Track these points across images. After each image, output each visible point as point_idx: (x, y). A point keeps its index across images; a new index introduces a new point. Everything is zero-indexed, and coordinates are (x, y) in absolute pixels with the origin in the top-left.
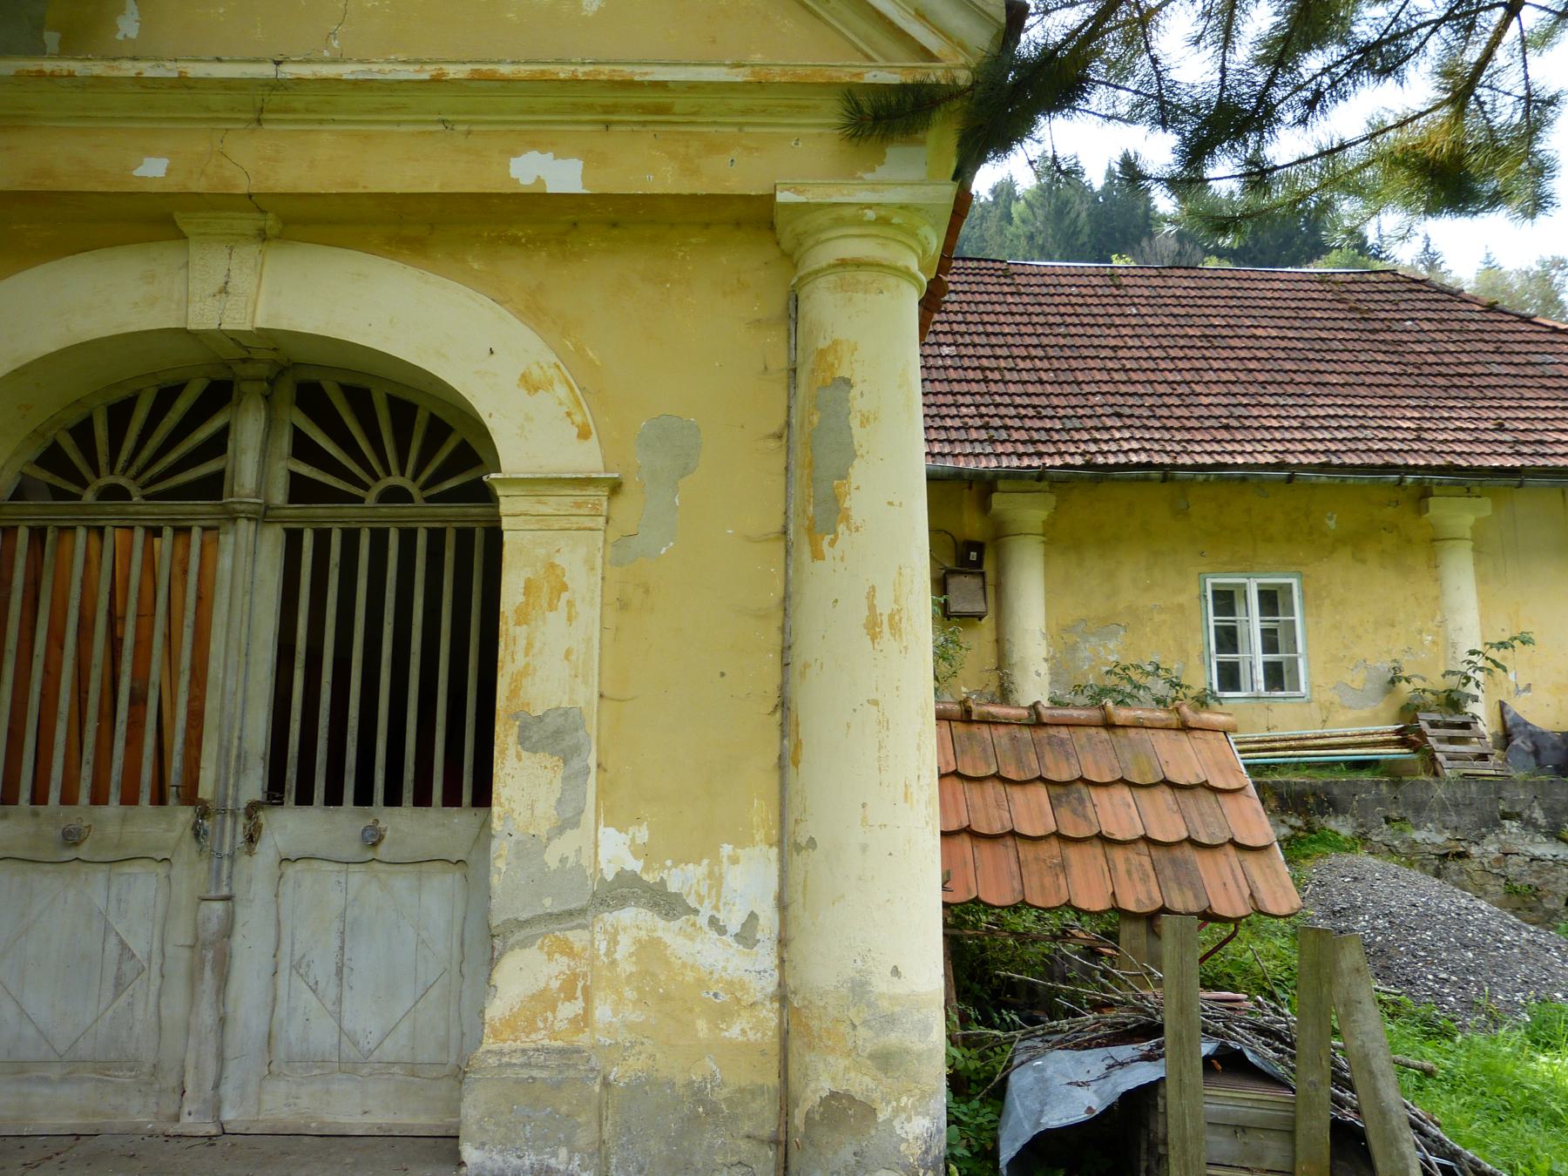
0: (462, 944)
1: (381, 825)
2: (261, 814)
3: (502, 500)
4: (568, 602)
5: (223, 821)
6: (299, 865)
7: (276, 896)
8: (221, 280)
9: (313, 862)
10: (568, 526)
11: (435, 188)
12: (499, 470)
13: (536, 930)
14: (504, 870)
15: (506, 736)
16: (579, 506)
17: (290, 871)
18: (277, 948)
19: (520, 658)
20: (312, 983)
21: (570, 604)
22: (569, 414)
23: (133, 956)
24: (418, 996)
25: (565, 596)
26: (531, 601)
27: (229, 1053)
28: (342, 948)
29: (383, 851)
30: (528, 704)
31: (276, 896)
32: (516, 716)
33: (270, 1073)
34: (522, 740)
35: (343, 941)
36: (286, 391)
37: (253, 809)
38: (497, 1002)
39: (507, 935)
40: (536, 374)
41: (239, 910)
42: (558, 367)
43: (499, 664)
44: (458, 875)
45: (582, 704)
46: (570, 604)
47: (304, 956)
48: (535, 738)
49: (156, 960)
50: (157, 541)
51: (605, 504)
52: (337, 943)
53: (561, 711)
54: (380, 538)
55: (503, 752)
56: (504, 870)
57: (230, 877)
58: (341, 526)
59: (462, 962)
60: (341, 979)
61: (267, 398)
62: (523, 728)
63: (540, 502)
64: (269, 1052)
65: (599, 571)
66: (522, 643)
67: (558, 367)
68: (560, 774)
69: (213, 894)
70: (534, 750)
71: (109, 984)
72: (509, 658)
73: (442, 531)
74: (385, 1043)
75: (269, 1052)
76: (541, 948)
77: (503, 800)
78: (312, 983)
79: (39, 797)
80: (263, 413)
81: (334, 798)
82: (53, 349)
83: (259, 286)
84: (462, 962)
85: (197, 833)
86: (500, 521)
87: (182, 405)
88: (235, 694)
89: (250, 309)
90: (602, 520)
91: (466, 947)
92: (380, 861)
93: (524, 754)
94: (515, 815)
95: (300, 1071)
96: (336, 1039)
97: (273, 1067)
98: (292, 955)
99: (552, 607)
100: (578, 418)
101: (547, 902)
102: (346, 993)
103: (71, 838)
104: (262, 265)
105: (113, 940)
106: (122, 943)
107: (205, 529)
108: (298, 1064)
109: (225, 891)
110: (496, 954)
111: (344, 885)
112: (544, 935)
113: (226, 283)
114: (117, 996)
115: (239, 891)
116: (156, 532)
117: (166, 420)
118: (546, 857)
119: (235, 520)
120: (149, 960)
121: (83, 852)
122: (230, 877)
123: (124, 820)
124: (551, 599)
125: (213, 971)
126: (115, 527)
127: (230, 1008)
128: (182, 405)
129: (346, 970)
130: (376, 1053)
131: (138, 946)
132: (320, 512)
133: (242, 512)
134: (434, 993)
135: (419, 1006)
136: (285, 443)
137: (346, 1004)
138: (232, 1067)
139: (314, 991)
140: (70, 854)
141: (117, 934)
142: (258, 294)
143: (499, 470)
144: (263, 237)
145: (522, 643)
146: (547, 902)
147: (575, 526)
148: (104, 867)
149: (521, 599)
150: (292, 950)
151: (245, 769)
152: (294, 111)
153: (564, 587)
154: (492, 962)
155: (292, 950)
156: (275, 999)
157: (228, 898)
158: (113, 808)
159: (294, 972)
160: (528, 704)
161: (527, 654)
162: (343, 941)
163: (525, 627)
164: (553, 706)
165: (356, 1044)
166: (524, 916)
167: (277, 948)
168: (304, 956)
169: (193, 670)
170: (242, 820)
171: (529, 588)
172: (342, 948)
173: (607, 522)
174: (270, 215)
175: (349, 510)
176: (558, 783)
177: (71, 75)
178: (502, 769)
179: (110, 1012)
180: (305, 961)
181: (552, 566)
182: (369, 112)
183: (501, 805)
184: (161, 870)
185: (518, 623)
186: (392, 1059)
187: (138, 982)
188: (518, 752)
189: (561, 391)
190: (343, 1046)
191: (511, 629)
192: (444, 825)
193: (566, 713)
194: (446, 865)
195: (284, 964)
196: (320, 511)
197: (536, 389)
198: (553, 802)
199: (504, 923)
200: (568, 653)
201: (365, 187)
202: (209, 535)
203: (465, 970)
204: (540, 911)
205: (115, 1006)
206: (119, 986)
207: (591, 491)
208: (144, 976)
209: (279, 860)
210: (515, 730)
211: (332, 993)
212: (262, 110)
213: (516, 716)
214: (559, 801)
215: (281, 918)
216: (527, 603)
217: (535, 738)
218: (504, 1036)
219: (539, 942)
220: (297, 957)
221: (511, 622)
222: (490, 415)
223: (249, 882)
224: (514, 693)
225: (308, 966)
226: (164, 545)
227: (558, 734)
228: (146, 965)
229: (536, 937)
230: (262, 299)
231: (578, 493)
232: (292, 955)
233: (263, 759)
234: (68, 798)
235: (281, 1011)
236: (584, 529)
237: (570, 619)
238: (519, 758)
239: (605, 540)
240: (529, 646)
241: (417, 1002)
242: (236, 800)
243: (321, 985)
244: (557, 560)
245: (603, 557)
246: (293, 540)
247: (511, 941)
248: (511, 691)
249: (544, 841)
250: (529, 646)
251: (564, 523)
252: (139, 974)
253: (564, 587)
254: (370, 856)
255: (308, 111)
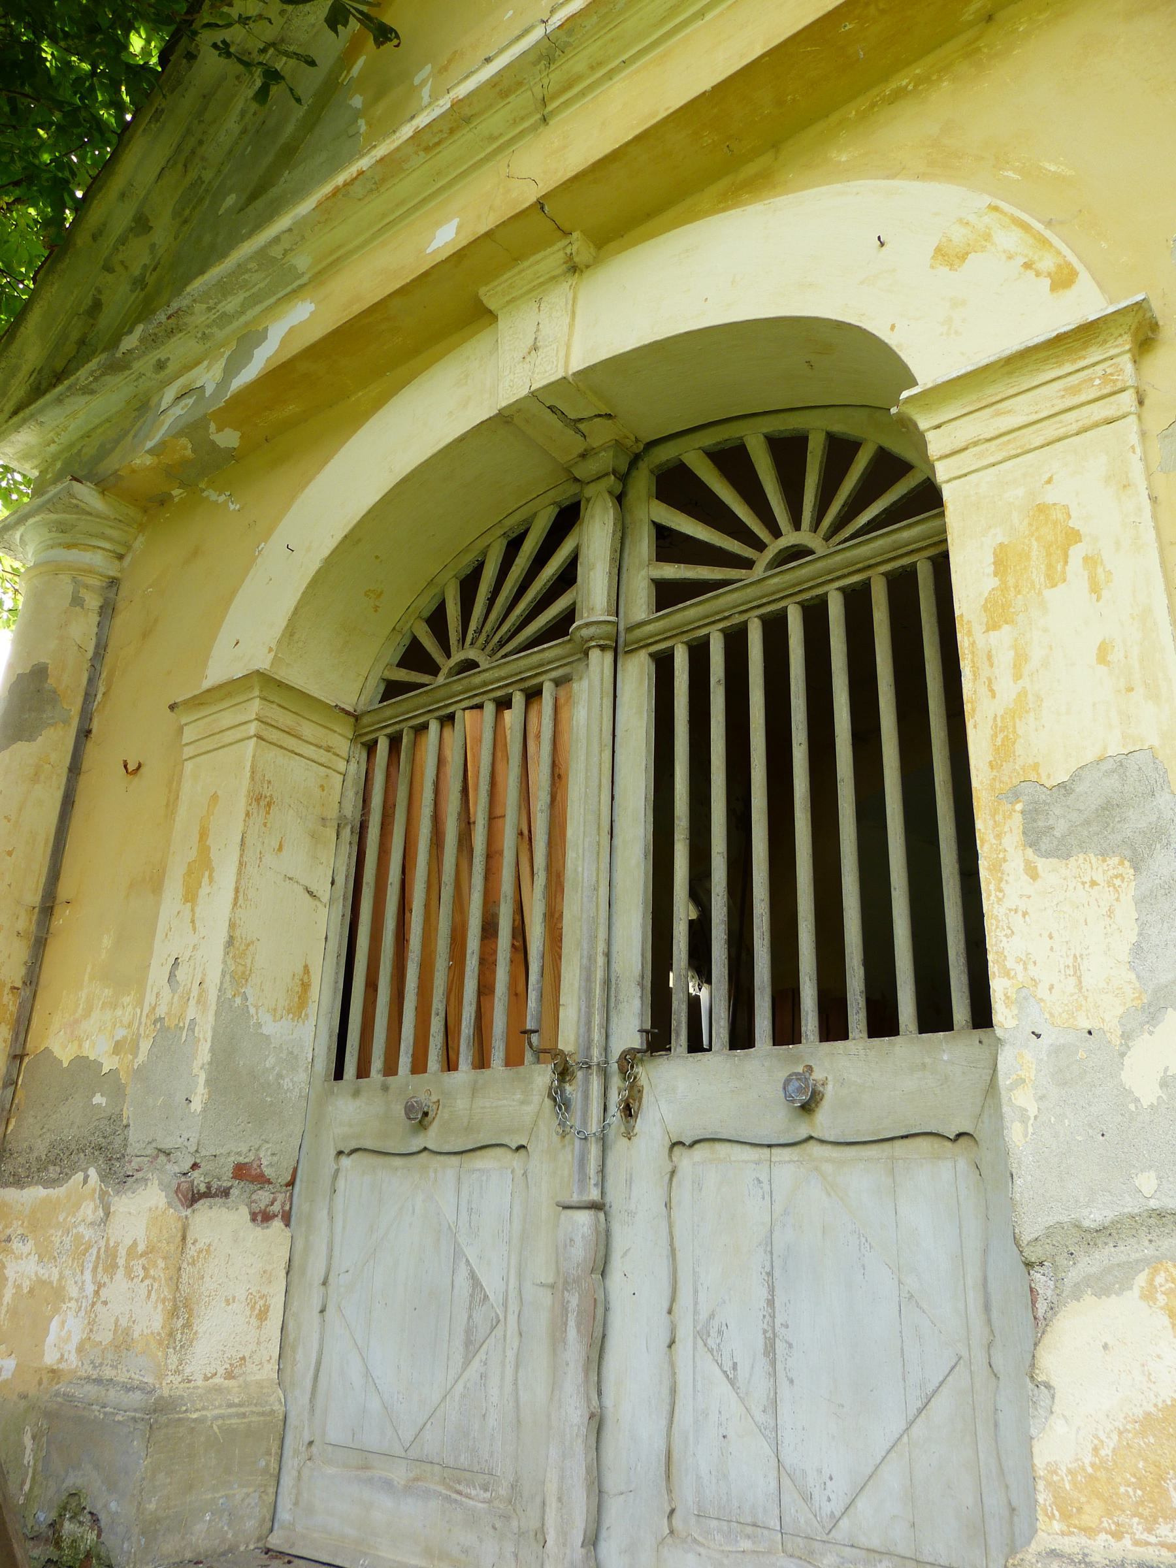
0: (987, 1307)
1: (818, 1075)
2: (639, 1070)
3: (929, 436)
4: (1086, 559)
5: (587, 1081)
6: (700, 1152)
7: (668, 1205)
8: (530, 342)
9: (718, 1146)
10: (1062, 432)
11: (758, 51)
12: (915, 383)
13: (1126, 1252)
14: (1032, 1111)
15: (999, 836)
16: (1073, 390)
17: (687, 1161)
18: (673, 1300)
19: (1007, 689)
20: (727, 1366)
21: (1091, 562)
22: (1027, 266)
23: (486, 1297)
24: (912, 1411)
25: (1077, 553)
26: (1011, 581)
27: (613, 1482)
28: (771, 1303)
29: (824, 1122)
30: (1036, 767)
31: (668, 1205)
32: (1015, 794)
33: (672, 1532)
34: (1034, 837)
35: (772, 1290)
36: (642, 483)
37: (629, 1060)
38: (1058, 1427)
39: (1062, 1260)
40: (959, 235)
41: (616, 1228)
42: (996, 209)
43: (967, 707)
44: (962, 1164)
45: (1155, 741)
46: (1091, 562)
47: (712, 1316)
48: (1061, 828)
49: (513, 1307)
50: (507, 713)
51: (1129, 367)
52: (764, 1293)
53: (1108, 765)
54: (775, 628)
55: (996, 868)
56: (1032, 1111)
57: (602, 1170)
58: (721, 625)
59: (989, 1346)
60: (773, 1363)
61: (620, 499)
62: (1032, 814)
63: (998, 414)
64: (670, 1491)
65: (1142, 486)
66: (1005, 658)
67: (996, 209)
68: (1129, 891)
69: (575, 1199)
70: (1062, 852)
71: (458, 1342)
72: (983, 690)
73: (866, 586)
74: (860, 1504)
75: (670, 1491)
76: (1148, 1296)
77: (1010, 963)
78: (727, 1366)
79: (390, 1069)
80: (611, 511)
81: (741, 1038)
82: (377, 498)
83: (571, 325)
84: (989, 1346)
85: (560, 1102)
86: (932, 468)
87: (529, 548)
88: (596, 889)
89: (562, 354)
90: (1127, 400)
91: (995, 1314)
92: (822, 1142)
93: (1041, 864)
94: (1042, 991)
95: (718, 1537)
96: (773, 1484)
97: (677, 1521)
98: (696, 1312)
99: (1053, 579)
100: (1047, 263)
101: (1147, 1182)
102: (785, 1391)
103: (421, 1118)
104: (574, 301)
105: (463, 1272)
106: (473, 1276)
107: (558, 683)
108: (714, 1523)
109: (594, 1195)
110: (1042, 1307)
111: (766, 1187)
112: (1152, 1262)
113: (536, 339)
114: (467, 1363)
115: (615, 1198)
116: (504, 704)
117: (514, 568)
118: (1127, 1077)
119: (586, 654)
120: (505, 1305)
121: (430, 1139)
122: (602, 1170)
123: (474, 1090)
124: (1050, 566)
125: (578, 1326)
126: (464, 709)
127: (609, 1401)
128: (529, 548)
129: (780, 1347)
130: (844, 1523)
131: (492, 1284)
132: (692, 613)
133: (592, 639)
134: (942, 1405)
135: (915, 1430)
136: (643, 545)
137: (784, 1410)
138: (615, 1509)
139: (732, 1382)
140: (417, 1143)
141: (467, 1261)
142: (570, 335)
143: (915, 383)
144: (574, 268)
145: (1005, 658)
146: (1147, 1182)
147: (1075, 427)
148: (454, 1160)
149: (994, 582)
150: (696, 1304)
151: (617, 1002)
152: (579, 78)
153: (1074, 536)
154: (1039, 1325)
155: (696, 1304)
156: (673, 1391)
157: (597, 1206)
158: (465, 1072)
159: (700, 1343)
160: (1036, 767)
161: (1018, 676)
162: (772, 1290)
163: (1006, 628)
164: (1089, 757)
165: (807, 1498)
166: (1094, 1217)
167: (673, 1300)
168: (712, 1316)
169: (549, 868)
170: (616, 1082)
171: (1001, 564)
172: (771, 1303)
173: (1141, 403)
174: (575, 235)
175: (724, 600)
176: (1127, 911)
177: (361, 173)
178: (999, 901)
179: (460, 1387)
180: (715, 1323)
181: (1042, 509)
182: (662, 21)
183: (1007, 974)
184: (516, 1161)
185: (992, 626)
186: (875, 1543)
187: (491, 1341)
188: (1028, 863)
189: (1009, 239)
190: (786, 1498)
191: (981, 641)
192: (924, 1065)
193: (1120, 765)
194: (936, 1143)
195: (685, 1332)
196: (690, 612)
197: (963, 257)
198: (1123, 951)
199: (1050, 1232)
200: (1103, 653)
201: (666, 110)
202: (562, 692)
203: (998, 1362)
204: (1130, 1206)
205: (466, 1375)
206: (471, 1347)
207: (1095, 354)
208: (499, 1332)
209: (668, 1144)
210: (1017, 821)
211: (760, 1388)
212: (544, 102)
213: (1015, 794)
214: (1137, 949)
215: (677, 1245)
216: (1004, 588)
217: (1061, 828)
218: (1090, 1517)
219: (1141, 1280)
220: (703, 1316)
221: (978, 629)
222: (893, 327)
223: (630, 1182)
224: (1003, 752)
225: (720, 1332)
226: (511, 718)
227: (1109, 811)
228: (501, 1317)
229: (1129, 1270)
230: (577, 337)
231: (1068, 368)
232: (696, 1312)
233: (642, 986)
234: (419, 1066)
235: (685, 1417)
236: (1096, 425)
237: (1095, 589)
238: (1032, 873)
239: (1143, 434)
240: (1020, 660)
241: (911, 1424)
242: (606, 1049)
243: (743, 1373)
244: (1051, 496)
245: (1145, 459)
246: (663, 665)
247: (1073, 1276)
248: (997, 750)
249: (1117, 1042)
250: (1020, 660)
251: (1051, 430)
252: (493, 1328)
253: (1074, 536)
254: (803, 1132)
255: (592, 68)
